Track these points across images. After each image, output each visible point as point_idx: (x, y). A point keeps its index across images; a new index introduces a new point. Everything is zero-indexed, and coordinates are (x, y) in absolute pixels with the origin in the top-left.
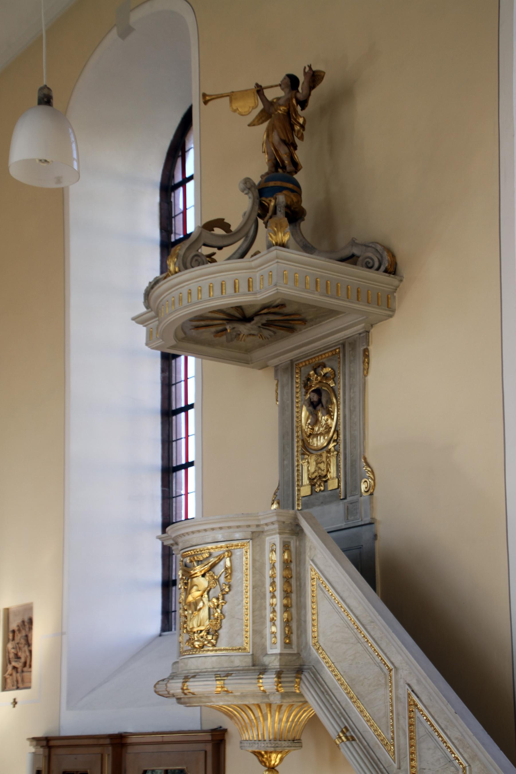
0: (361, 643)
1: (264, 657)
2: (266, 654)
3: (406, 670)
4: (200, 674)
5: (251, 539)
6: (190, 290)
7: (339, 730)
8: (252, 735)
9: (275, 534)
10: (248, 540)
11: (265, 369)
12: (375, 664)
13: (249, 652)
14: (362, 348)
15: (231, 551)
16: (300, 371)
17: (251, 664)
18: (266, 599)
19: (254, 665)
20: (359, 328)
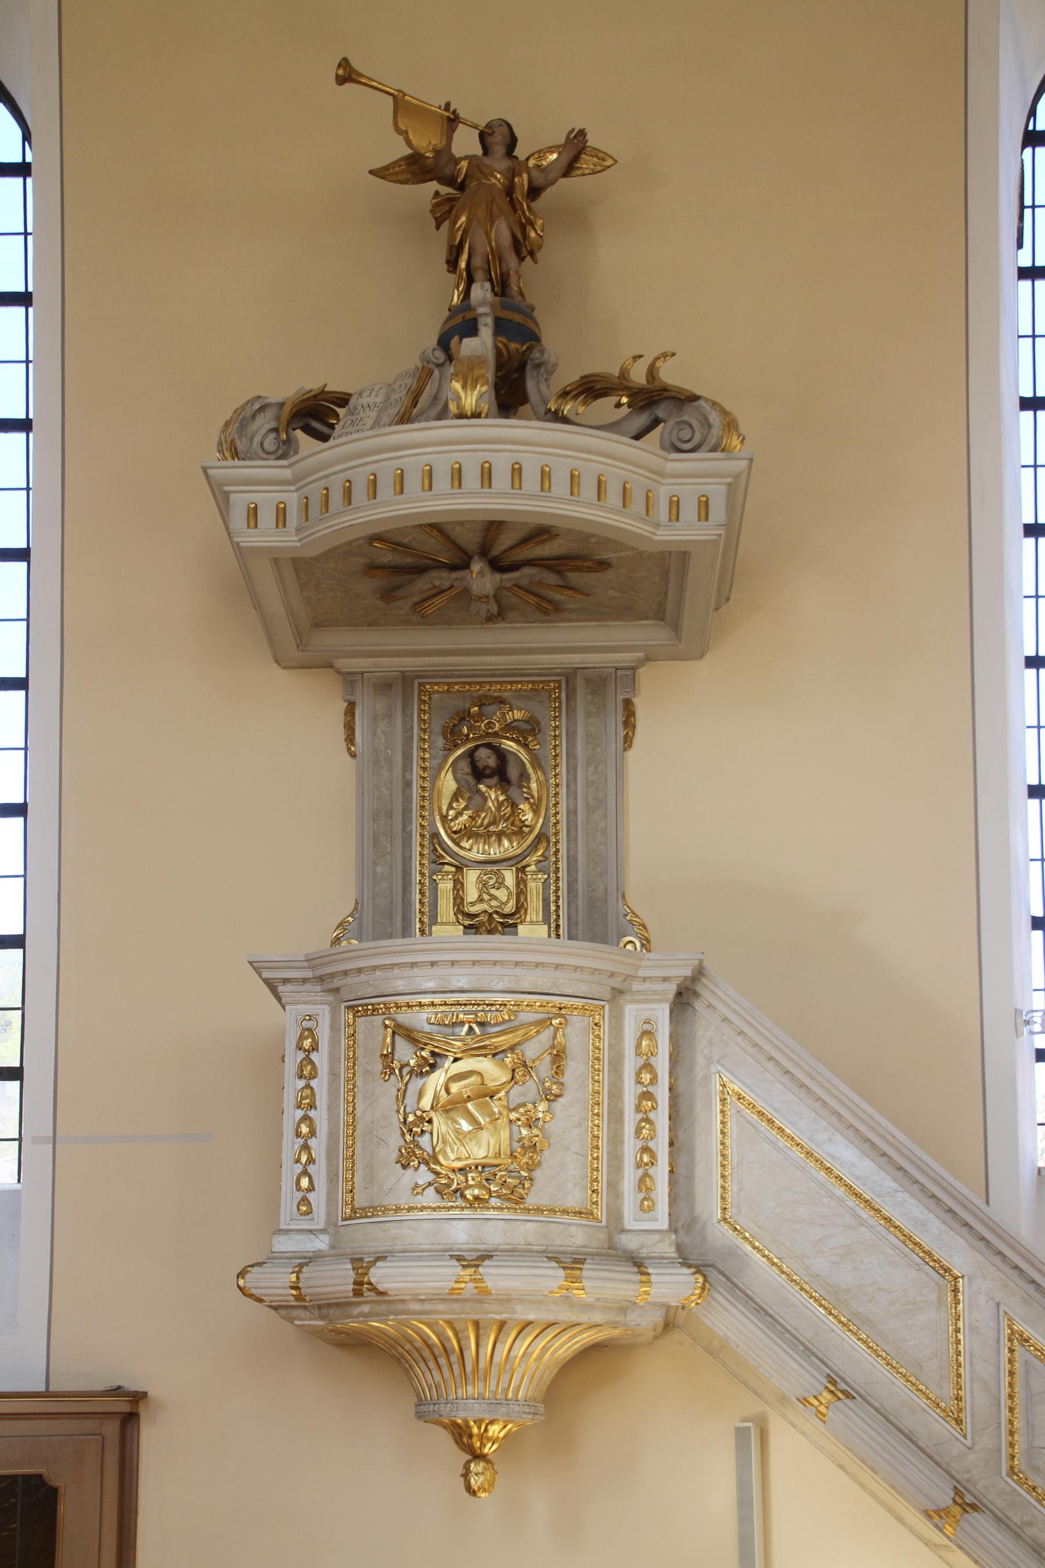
0: (867, 1225)
1: (274, 1234)
2: (623, 1231)
3: (993, 1280)
4: (395, 1254)
5: (608, 1001)
6: (349, 481)
7: (825, 1381)
8: (506, 1386)
9: (660, 1001)
10: (603, 1003)
11: (289, 670)
12: (912, 1266)
13: (601, 1222)
14: (621, 697)
15: (567, 1016)
16: (430, 699)
17: (606, 1246)
18: (624, 1124)
19: (610, 1248)
20: (627, 658)
